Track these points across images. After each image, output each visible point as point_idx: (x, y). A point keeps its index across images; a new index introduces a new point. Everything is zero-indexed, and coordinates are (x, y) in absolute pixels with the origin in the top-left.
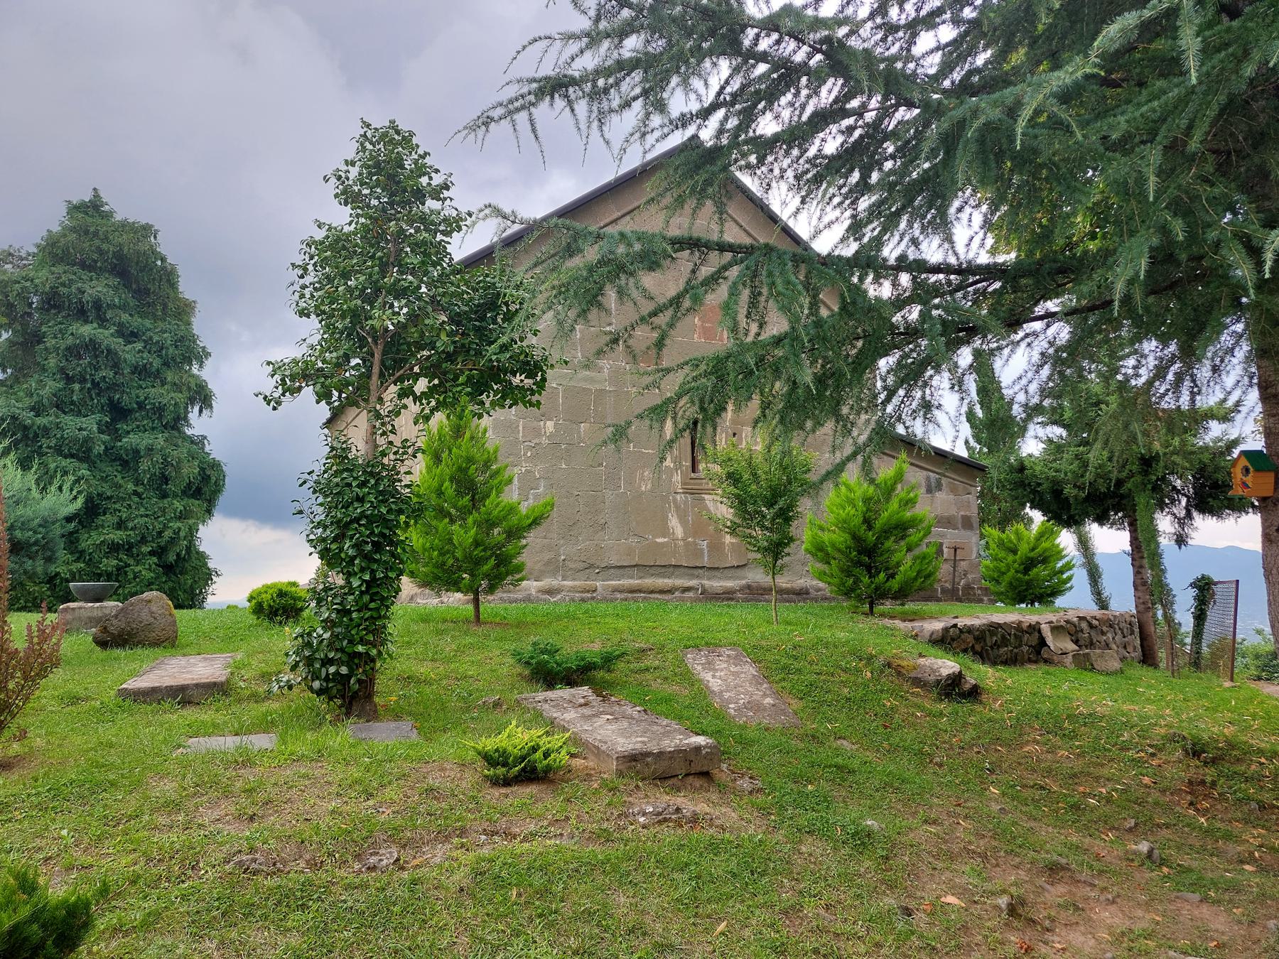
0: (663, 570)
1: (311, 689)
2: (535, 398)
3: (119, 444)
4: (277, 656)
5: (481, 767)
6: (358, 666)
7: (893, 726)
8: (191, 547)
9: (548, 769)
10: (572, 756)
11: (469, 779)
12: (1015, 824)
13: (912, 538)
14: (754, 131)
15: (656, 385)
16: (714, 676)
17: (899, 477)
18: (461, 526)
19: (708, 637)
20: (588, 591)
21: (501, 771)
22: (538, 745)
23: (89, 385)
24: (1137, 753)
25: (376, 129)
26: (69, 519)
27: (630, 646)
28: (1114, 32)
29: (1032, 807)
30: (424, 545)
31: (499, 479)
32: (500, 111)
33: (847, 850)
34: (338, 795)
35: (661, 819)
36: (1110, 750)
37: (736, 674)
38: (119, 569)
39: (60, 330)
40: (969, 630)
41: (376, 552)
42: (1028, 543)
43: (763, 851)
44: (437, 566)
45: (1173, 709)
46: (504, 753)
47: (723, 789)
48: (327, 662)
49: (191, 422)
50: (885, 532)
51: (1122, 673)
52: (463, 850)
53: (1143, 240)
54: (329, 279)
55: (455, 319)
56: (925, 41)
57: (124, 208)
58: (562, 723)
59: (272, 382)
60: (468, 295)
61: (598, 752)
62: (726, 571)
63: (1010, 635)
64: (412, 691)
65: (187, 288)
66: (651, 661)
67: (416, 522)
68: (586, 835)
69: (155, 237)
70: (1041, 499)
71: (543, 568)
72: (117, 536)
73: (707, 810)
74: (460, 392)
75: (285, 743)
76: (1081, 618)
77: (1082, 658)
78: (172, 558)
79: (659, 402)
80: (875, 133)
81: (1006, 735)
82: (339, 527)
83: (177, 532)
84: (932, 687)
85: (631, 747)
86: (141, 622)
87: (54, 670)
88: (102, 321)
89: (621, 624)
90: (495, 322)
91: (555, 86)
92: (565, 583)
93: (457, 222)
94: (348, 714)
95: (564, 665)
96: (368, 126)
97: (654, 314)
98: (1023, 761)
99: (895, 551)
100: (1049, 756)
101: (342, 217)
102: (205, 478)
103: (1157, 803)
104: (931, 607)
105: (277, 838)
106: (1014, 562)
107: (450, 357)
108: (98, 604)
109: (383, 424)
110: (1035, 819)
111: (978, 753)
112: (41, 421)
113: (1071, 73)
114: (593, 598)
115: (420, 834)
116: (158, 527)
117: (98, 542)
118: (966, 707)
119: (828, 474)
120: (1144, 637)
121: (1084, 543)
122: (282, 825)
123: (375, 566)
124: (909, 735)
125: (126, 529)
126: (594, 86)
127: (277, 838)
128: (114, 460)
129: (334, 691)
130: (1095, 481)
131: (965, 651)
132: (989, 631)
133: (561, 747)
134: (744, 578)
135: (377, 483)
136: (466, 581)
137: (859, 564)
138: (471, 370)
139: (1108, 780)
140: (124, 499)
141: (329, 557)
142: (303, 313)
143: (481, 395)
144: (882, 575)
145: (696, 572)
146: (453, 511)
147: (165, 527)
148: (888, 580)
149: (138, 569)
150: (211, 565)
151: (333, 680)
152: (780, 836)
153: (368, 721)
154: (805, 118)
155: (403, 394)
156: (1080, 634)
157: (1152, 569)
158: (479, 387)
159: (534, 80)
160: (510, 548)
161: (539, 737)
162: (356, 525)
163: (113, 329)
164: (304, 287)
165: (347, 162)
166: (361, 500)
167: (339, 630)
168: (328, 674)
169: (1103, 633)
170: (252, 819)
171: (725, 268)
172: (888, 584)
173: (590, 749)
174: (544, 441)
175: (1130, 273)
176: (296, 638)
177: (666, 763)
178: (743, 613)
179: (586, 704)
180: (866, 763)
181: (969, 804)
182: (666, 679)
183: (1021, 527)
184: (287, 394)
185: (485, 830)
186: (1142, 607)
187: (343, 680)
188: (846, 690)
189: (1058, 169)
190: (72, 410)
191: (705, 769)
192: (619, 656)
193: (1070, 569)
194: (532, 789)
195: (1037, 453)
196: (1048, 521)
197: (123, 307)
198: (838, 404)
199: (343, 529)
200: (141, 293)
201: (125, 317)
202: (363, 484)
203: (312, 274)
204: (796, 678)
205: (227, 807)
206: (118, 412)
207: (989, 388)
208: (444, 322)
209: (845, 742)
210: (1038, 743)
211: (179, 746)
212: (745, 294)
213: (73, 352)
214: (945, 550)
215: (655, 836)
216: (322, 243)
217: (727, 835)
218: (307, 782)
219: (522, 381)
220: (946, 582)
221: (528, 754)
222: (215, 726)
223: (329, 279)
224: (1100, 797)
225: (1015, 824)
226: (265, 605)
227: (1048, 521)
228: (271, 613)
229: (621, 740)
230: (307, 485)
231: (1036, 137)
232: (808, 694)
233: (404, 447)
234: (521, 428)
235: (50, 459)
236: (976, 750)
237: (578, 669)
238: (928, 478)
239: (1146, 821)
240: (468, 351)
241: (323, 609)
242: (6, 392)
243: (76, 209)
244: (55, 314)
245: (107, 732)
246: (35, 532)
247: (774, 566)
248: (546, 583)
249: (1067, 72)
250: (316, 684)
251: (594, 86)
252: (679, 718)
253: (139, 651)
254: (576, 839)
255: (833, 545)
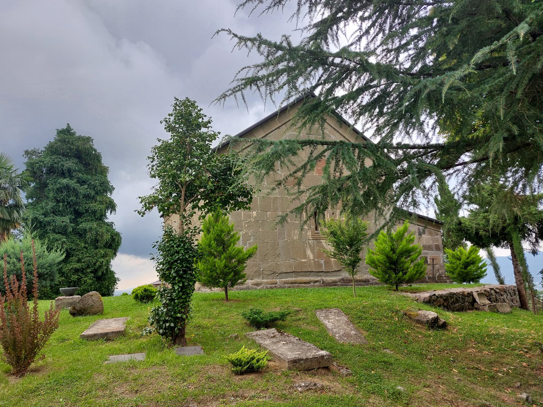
0: (305, 274)
1: (159, 333)
2: (248, 206)
3: (78, 227)
4: (145, 318)
5: (230, 367)
6: (178, 323)
7: (409, 342)
8: (108, 269)
9: (259, 367)
10: (269, 361)
11: (226, 372)
12: (465, 386)
13: (413, 256)
14: (334, 95)
15: (298, 198)
16: (329, 322)
17: (406, 230)
18: (219, 259)
19: (326, 304)
20: (273, 284)
21: (239, 368)
22: (254, 357)
23: (66, 204)
24: (519, 351)
25: (180, 101)
26: (59, 263)
27: (292, 310)
28: (479, 55)
29: (473, 378)
30: (204, 268)
31: (234, 239)
32: (230, 92)
33: (389, 401)
34: (172, 380)
35: (308, 388)
36: (507, 351)
37: (338, 321)
38: (78, 279)
39: (54, 182)
40: (441, 296)
41: (184, 274)
42: (465, 256)
43: (353, 402)
44: (209, 277)
45: (535, 330)
46: (240, 360)
47: (334, 374)
48: (165, 321)
49: (107, 217)
50: (401, 254)
51: (512, 313)
52: (224, 404)
53: (500, 134)
54: (163, 162)
55: (215, 176)
56: (402, 57)
57: (80, 130)
58: (264, 346)
59: (141, 205)
60: (217, 162)
61: (280, 359)
62: (332, 273)
63: (459, 298)
64: (200, 332)
65: (105, 162)
66: (300, 316)
67: (200, 261)
68: (276, 397)
69: (92, 142)
70: (470, 236)
71: (254, 274)
72: (78, 266)
73: (328, 384)
74: (217, 205)
75: (149, 358)
76: (491, 289)
77: (492, 307)
78: (100, 274)
79: (299, 205)
80: (385, 94)
81: (459, 345)
82: (169, 264)
83: (102, 263)
84: (425, 324)
85: (294, 356)
86: (89, 305)
87: (56, 330)
88: (71, 177)
89: (288, 299)
90: (231, 176)
91: (252, 81)
92: (263, 280)
93: (214, 136)
94: (174, 344)
95: (264, 319)
96: (177, 100)
97: (295, 172)
98: (467, 356)
99: (406, 262)
100: (479, 354)
101: (168, 137)
102: (113, 240)
103: (530, 375)
104: (424, 286)
105: (147, 400)
106: (460, 264)
107: (213, 192)
108: (71, 297)
109: (186, 221)
110: (474, 384)
111: (447, 353)
112: (46, 219)
113: (463, 72)
114: (276, 287)
115: (206, 397)
116: (94, 261)
117: (70, 268)
118: (441, 332)
119: (373, 235)
120: (521, 296)
121: (491, 255)
122: (149, 395)
123: (184, 280)
124: (416, 346)
125: (81, 262)
126: (268, 80)
127: (147, 400)
128: (76, 234)
129: (169, 334)
130: (493, 228)
131: (439, 306)
132: (450, 296)
133: (264, 357)
134: (341, 276)
135: (184, 245)
136: (222, 283)
137: (390, 268)
138: (221, 196)
139: (507, 364)
140: (80, 250)
141: (164, 276)
142: (153, 176)
143: (226, 206)
144: (401, 273)
145: (320, 274)
146: (215, 253)
147: (97, 261)
148: (403, 275)
149: (85, 279)
150: (116, 276)
151: (168, 329)
152: (360, 395)
153: (183, 346)
154: (354, 89)
155: (194, 207)
156: (491, 296)
157: (522, 265)
158: (225, 203)
159: (243, 79)
160: (239, 268)
161: (254, 353)
162: (176, 263)
163: (75, 180)
164: (153, 166)
165: (169, 115)
166: (178, 252)
167: (170, 307)
168: (166, 327)
169: (502, 295)
170: (136, 392)
171: (324, 152)
172: (404, 277)
173: (276, 357)
174: (252, 220)
175: (495, 149)
176: (152, 312)
177: (309, 363)
178: (341, 292)
179: (274, 337)
180: (397, 360)
181: (444, 378)
182: (308, 323)
183: (462, 248)
184: (147, 210)
185: (233, 395)
186: (519, 283)
187: (172, 329)
188: (387, 327)
189: (462, 105)
190: (59, 214)
191: (326, 365)
192: (287, 314)
193: (485, 266)
194: (252, 376)
195: (466, 216)
196: (474, 246)
197: (79, 171)
198: (376, 203)
199: (171, 265)
200: (87, 165)
201: (80, 175)
202: (178, 246)
203: (156, 160)
204: (365, 322)
205: (127, 387)
206: (78, 214)
207: (443, 189)
208: (209, 177)
209: (387, 350)
210: (474, 348)
211: (106, 360)
212: (333, 163)
213: (60, 190)
214: (429, 260)
215: (306, 397)
216: (160, 147)
217: (337, 395)
218: (159, 375)
219: (242, 199)
220: (430, 274)
221: (250, 361)
222: (120, 350)
223: (163, 162)
224: (503, 373)
225: (465, 386)
226: (139, 295)
227: (474, 246)
228: (141, 298)
229: (289, 353)
230: (156, 247)
231: (452, 94)
232: (370, 329)
233: (195, 230)
234: (242, 215)
235: (51, 235)
236: (446, 352)
237: (270, 321)
238: (419, 229)
239: (525, 383)
240: (220, 188)
241: (163, 299)
242: (33, 208)
243: (61, 132)
244: (52, 175)
245: (76, 354)
246: (46, 269)
247: (353, 271)
248: (256, 280)
249: (461, 71)
250: (161, 331)
251: (268, 80)
252: (314, 341)
253: (88, 317)
254: (272, 398)
255: (378, 261)
